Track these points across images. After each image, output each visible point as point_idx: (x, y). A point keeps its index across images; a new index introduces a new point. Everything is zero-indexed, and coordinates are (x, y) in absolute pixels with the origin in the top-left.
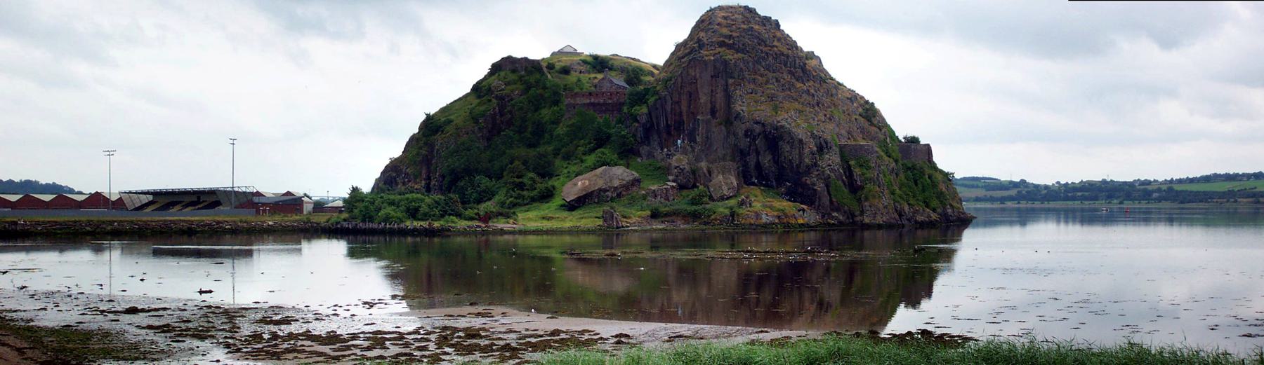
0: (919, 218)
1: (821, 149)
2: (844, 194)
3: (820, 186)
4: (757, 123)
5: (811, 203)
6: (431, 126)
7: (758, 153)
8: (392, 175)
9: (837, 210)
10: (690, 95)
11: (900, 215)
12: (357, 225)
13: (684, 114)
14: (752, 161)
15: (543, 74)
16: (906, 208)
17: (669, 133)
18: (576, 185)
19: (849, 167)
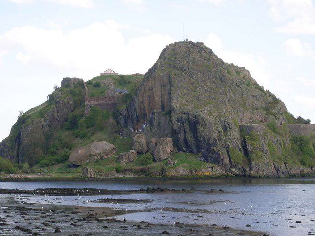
0: (293, 171)
1: (225, 129)
2: (239, 155)
3: (223, 152)
4: (185, 113)
5: (218, 163)
6: (23, 120)
7: (185, 132)
9: (235, 167)
11: (277, 170)
13: (146, 109)
14: (181, 136)
15: (84, 88)
16: (283, 166)
17: (138, 121)
18: (77, 152)
19: (244, 140)
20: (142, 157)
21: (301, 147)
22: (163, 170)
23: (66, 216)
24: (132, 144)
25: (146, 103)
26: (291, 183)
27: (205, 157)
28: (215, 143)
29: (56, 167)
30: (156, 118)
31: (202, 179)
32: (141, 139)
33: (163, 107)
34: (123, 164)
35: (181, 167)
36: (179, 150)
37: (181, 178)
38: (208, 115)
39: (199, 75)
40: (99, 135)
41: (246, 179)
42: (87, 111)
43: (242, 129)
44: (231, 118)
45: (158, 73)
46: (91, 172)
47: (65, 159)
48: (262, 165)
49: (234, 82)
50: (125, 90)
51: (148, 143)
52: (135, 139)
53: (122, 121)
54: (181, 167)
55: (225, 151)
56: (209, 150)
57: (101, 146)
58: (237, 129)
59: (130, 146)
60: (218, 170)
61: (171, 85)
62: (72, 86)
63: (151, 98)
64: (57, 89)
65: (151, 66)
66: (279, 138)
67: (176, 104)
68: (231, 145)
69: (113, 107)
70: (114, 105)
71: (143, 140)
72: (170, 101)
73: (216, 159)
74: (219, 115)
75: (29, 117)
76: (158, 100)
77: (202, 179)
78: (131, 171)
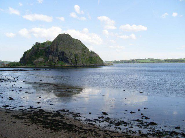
0: (88, 65)
1: (71, 55)
3: (70, 61)
5: (69, 63)
6: (26, 53)
9: (73, 64)
11: (83, 65)
14: (60, 57)
22: (55, 65)
24: (48, 59)
26: (87, 68)
28: (68, 58)
29: (30, 64)
30: (55, 53)
31: (64, 67)
32: (51, 57)
37: (59, 67)
39: (66, 42)
40: (41, 56)
41: (76, 67)
42: (39, 51)
43: (75, 55)
47: (32, 63)
48: (80, 63)
51: (52, 59)
55: (70, 60)
56: (66, 60)
57: (41, 59)
58: (74, 55)
59: (48, 59)
60: (69, 65)
61: (58, 44)
63: (54, 48)
65: (22, 56)
66: (85, 57)
67: (59, 49)
68: (72, 59)
73: (68, 62)
74: (69, 52)
76: (55, 48)
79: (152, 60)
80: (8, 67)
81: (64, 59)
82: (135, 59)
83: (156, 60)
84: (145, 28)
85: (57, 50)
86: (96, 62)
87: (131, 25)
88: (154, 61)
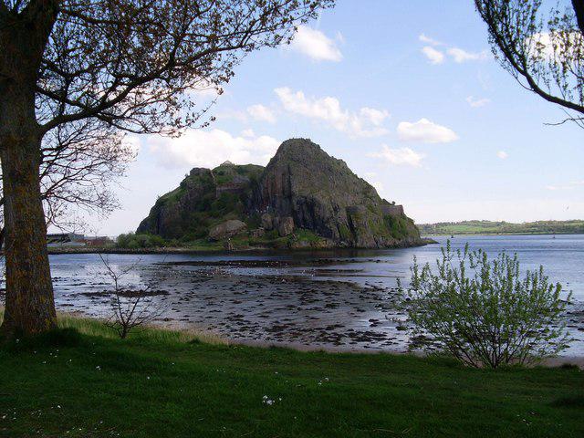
0: (388, 243)
1: (335, 209)
2: (346, 230)
5: (330, 237)
6: (161, 203)
8: (144, 226)
10: (272, 185)
12: (124, 246)
20: (270, 233)
21: (391, 224)
22: (289, 243)
23: (482, 232)
25: (270, 189)
27: (319, 232)
28: (328, 222)
30: (278, 201)
32: (267, 218)
33: (283, 192)
34: (254, 238)
35: (303, 241)
36: (299, 227)
38: (322, 198)
42: (218, 195)
43: (348, 210)
44: (339, 201)
45: (279, 164)
46: (231, 246)
47: (205, 234)
48: (366, 239)
49: (335, 170)
50: (247, 178)
52: (262, 218)
53: (249, 203)
54: (303, 241)
60: (331, 243)
62: (201, 175)
64: (187, 177)
65: (145, 213)
67: (296, 189)
69: (241, 192)
70: (241, 190)
71: (269, 219)
72: (290, 187)
73: (329, 235)
75: (166, 200)
77: (297, 251)
78: (261, 244)
79: (485, 224)
80: (121, 250)
81: (315, 225)
82: (431, 222)
83: (498, 224)
84: (444, 133)
85: (290, 196)
86: (406, 234)
87: (342, 110)
88: (496, 229)
